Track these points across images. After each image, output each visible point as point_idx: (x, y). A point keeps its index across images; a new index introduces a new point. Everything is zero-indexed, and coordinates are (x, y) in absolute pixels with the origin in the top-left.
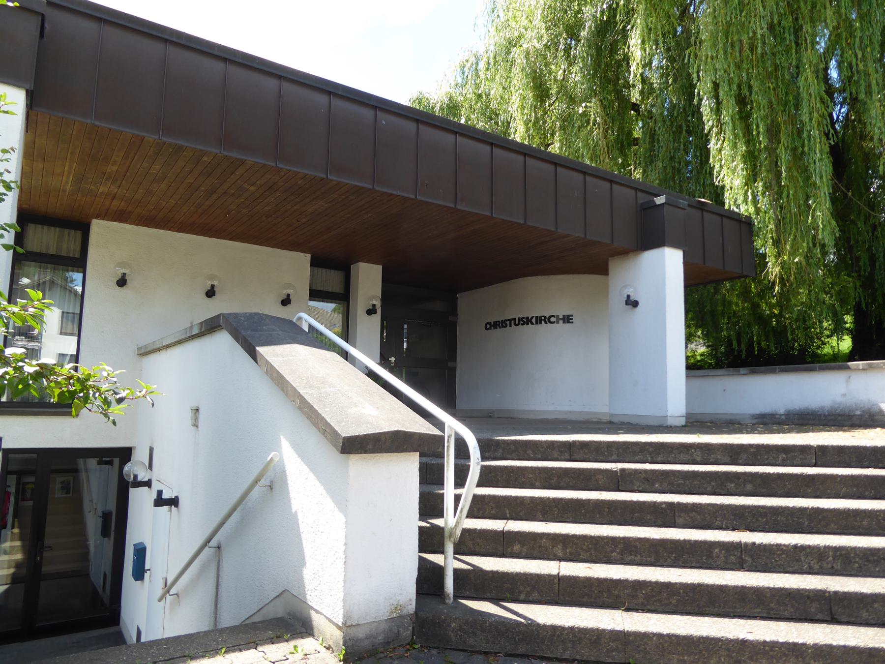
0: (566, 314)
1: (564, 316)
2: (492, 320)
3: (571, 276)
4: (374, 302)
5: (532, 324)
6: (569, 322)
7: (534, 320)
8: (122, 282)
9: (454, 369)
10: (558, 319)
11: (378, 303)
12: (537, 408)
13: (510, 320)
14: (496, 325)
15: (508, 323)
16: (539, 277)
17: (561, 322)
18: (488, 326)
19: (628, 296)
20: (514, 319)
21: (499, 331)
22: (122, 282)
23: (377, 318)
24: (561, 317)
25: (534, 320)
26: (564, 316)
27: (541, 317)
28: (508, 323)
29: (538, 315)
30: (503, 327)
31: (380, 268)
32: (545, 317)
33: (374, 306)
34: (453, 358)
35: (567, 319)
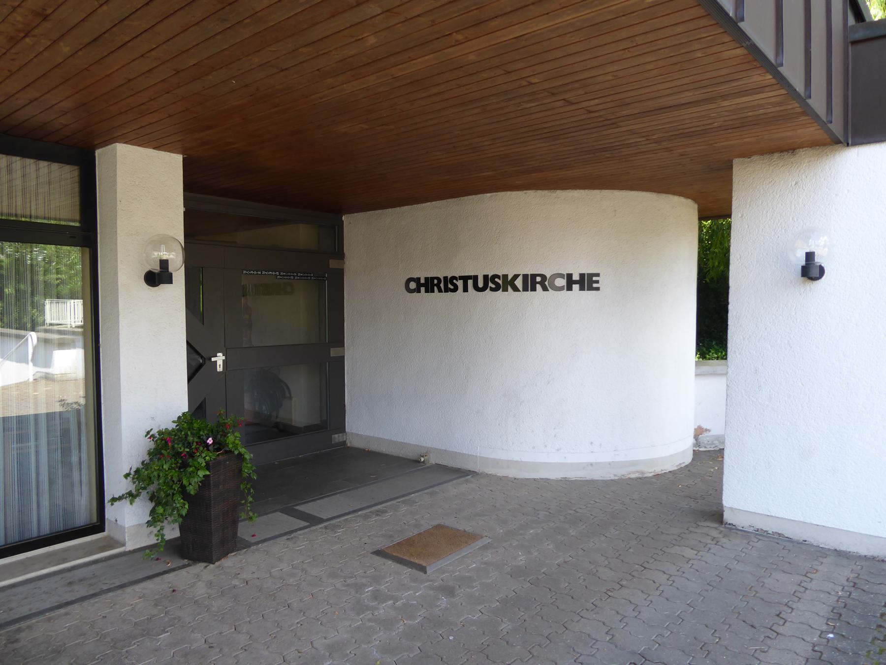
0: (586, 271)
1: (582, 276)
2: (422, 275)
3: (597, 192)
4: (165, 255)
5: (516, 289)
6: (591, 288)
7: (519, 283)
8: (811, 270)
9: (341, 360)
10: (570, 282)
11: (176, 258)
12: (515, 456)
13: (465, 279)
14: (430, 285)
15: (460, 283)
16: (531, 193)
17: (576, 287)
18: (413, 285)
19: (810, 256)
20: (475, 278)
21: (437, 298)
22: (811, 270)
23: (174, 296)
24: (576, 277)
25: (519, 283)
26: (582, 276)
27: (534, 276)
28: (460, 283)
29: (530, 271)
30: (447, 290)
31: (177, 160)
32: (543, 277)
33: (164, 264)
34: (338, 340)
35: (587, 282)
